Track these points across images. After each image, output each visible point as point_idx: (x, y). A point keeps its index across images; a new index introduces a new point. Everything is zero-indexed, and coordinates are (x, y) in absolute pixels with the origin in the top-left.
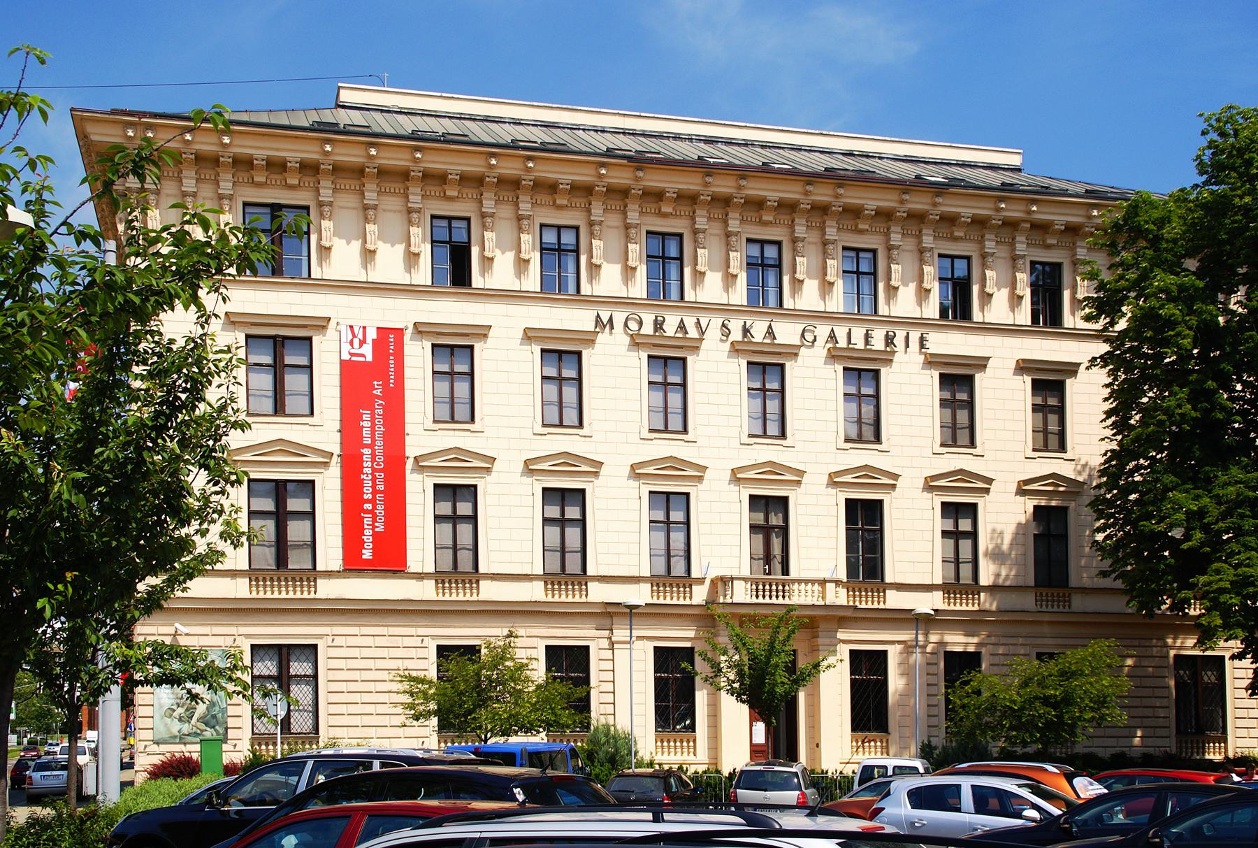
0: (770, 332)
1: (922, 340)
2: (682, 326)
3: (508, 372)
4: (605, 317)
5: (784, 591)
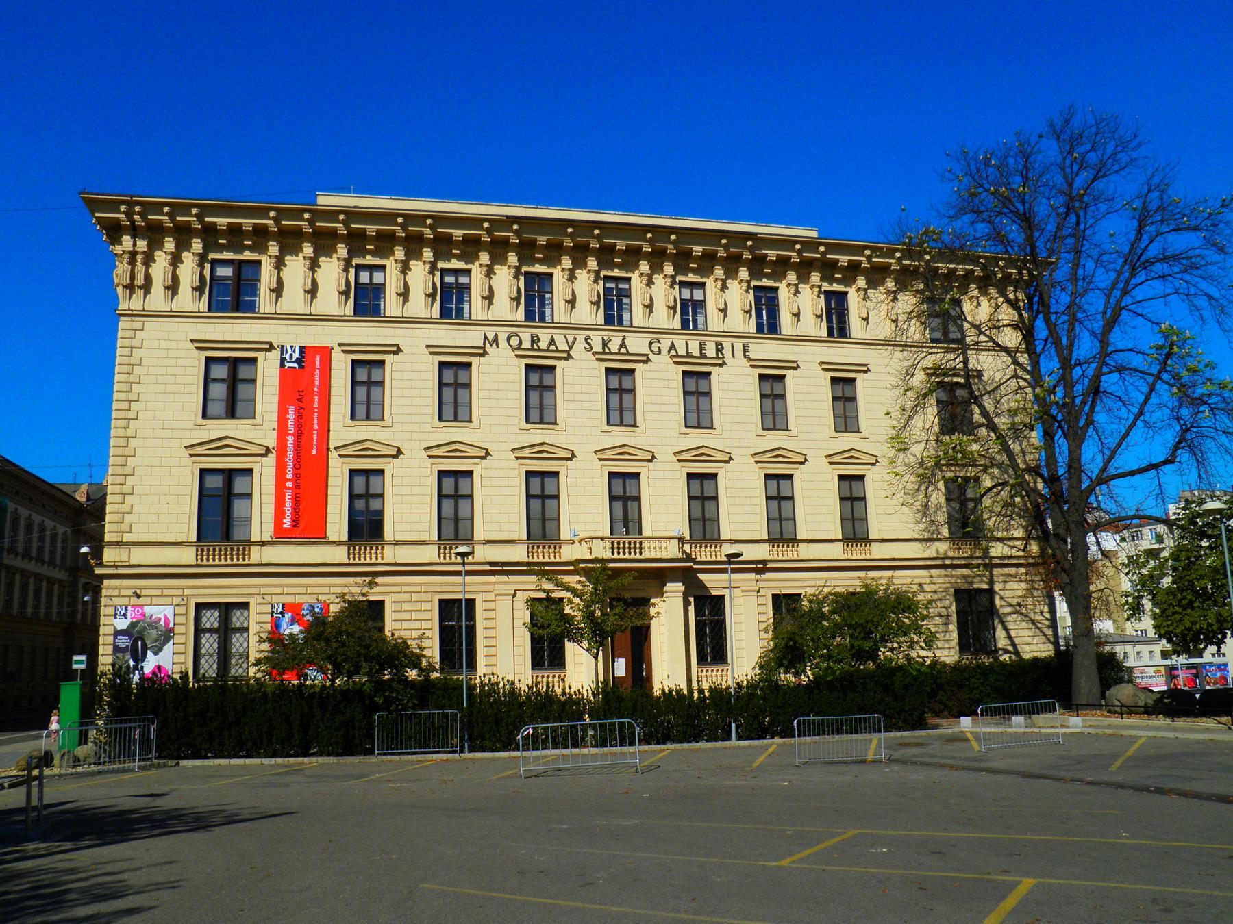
0: (623, 345)
1: (745, 346)
2: (552, 342)
3: (411, 384)
4: (491, 336)
5: (641, 548)
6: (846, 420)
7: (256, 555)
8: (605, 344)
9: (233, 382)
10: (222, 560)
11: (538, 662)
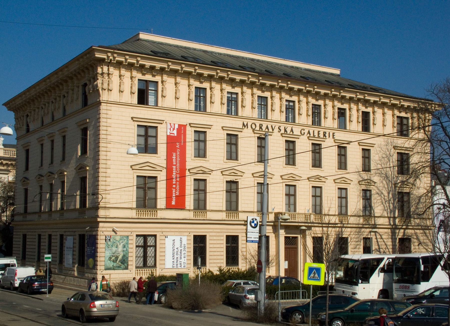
0: (292, 130)
2: (267, 127)
6: (317, 163)
7: (161, 214)
8: (285, 131)
9: (146, 136)
10: (146, 215)
11: (228, 264)
